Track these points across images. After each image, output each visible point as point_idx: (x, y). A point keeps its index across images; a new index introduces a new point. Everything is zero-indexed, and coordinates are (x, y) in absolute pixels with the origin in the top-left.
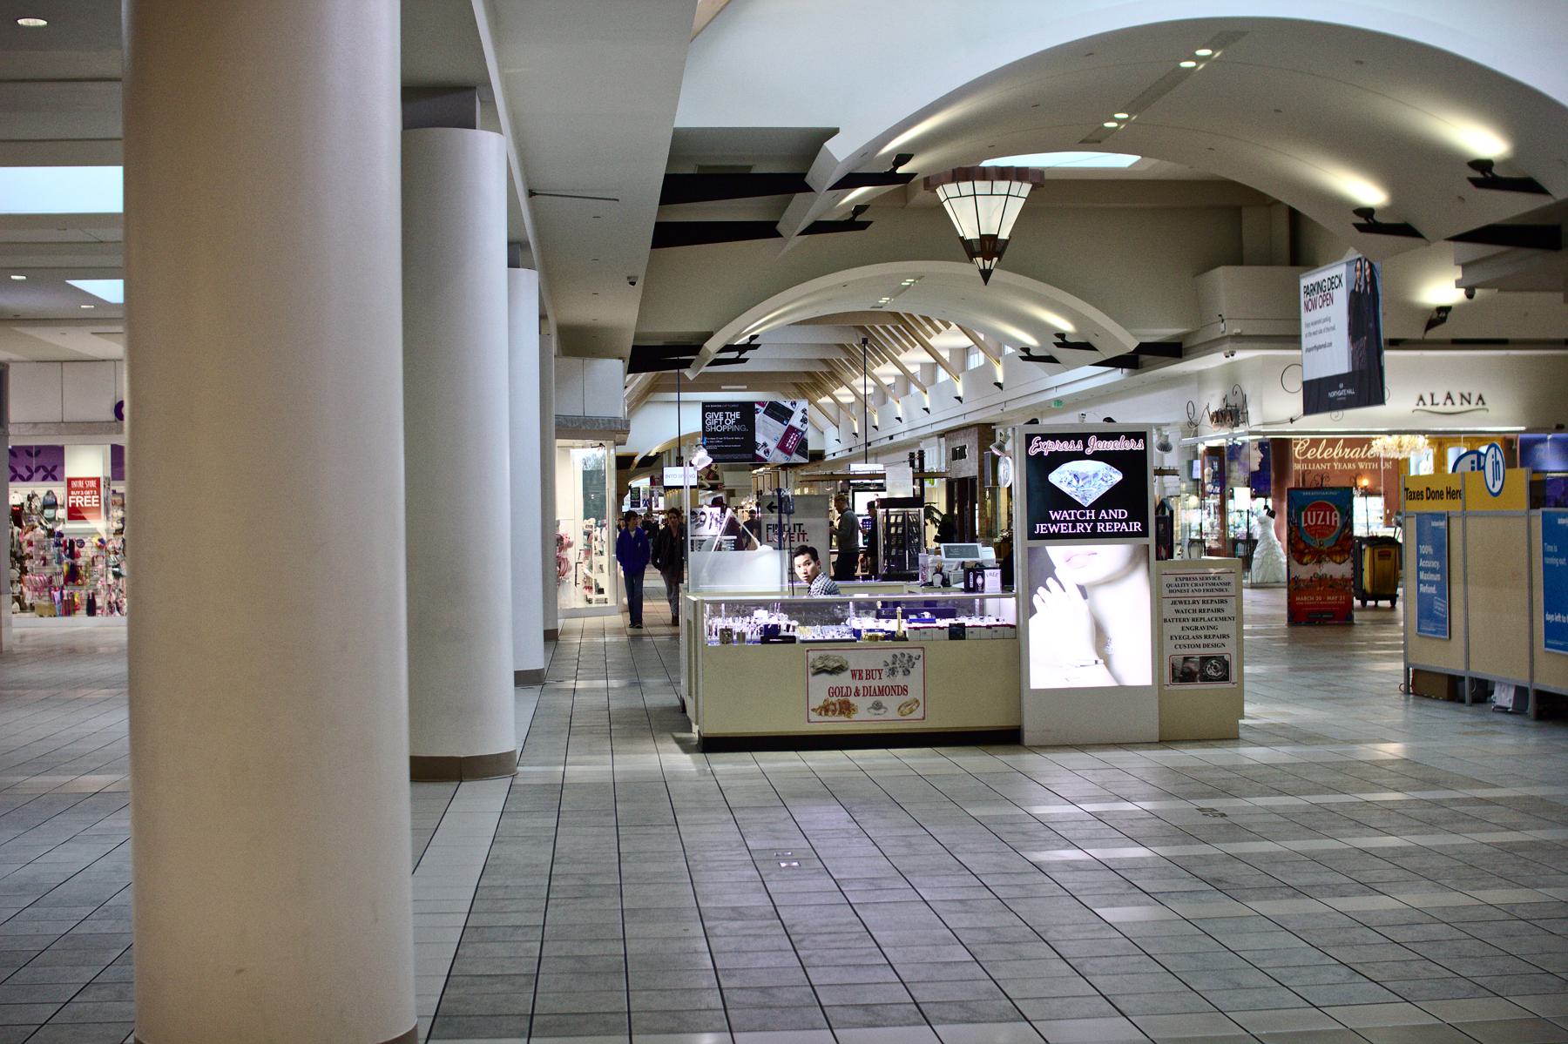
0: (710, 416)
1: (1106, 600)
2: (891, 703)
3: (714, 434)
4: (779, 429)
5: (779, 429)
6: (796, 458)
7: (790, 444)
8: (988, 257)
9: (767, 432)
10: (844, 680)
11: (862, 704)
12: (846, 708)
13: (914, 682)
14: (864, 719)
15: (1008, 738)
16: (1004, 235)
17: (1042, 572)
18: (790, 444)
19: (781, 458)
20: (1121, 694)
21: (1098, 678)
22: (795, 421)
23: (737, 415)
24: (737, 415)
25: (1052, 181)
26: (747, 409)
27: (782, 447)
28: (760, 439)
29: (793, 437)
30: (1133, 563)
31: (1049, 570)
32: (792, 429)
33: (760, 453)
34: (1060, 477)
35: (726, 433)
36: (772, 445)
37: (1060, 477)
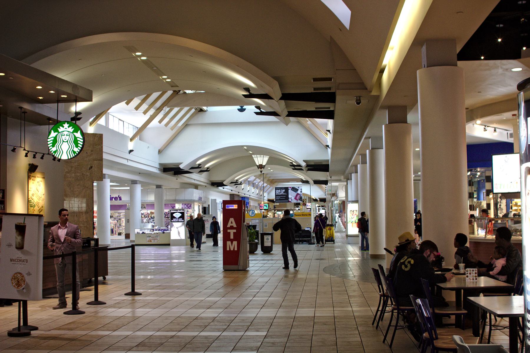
0: (277, 191)
1: (180, 229)
2: (156, 241)
3: (278, 195)
4: (295, 194)
5: (295, 194)
6: (299, 201)
7: (298, 198)
8: (261, 168)
9: (292, 195)
10: (151, 238)
11: (153, 241)
12: (151, 241)
13: (158, 238)
14: (153, 243)
15: (169, 245)
16: (264, 164)
17: (172, 226)
18: (298, 198)
19: (295, 201)
20: (181, 240)
21: (179, 238)
22: (299, 192)
23: (284, 190)
24: (284, 190)
25: (213, 168)
26: (287, 189)
27: (295, 198)
28: (290, 196)
29: (298, 196)
30: (183, 225)
31: (173, 225)
32: (298, 194)
33: (290, 200)
34: (174, 215)
35: (281, 195)
36: (293, 198)
37: (174, 215)
